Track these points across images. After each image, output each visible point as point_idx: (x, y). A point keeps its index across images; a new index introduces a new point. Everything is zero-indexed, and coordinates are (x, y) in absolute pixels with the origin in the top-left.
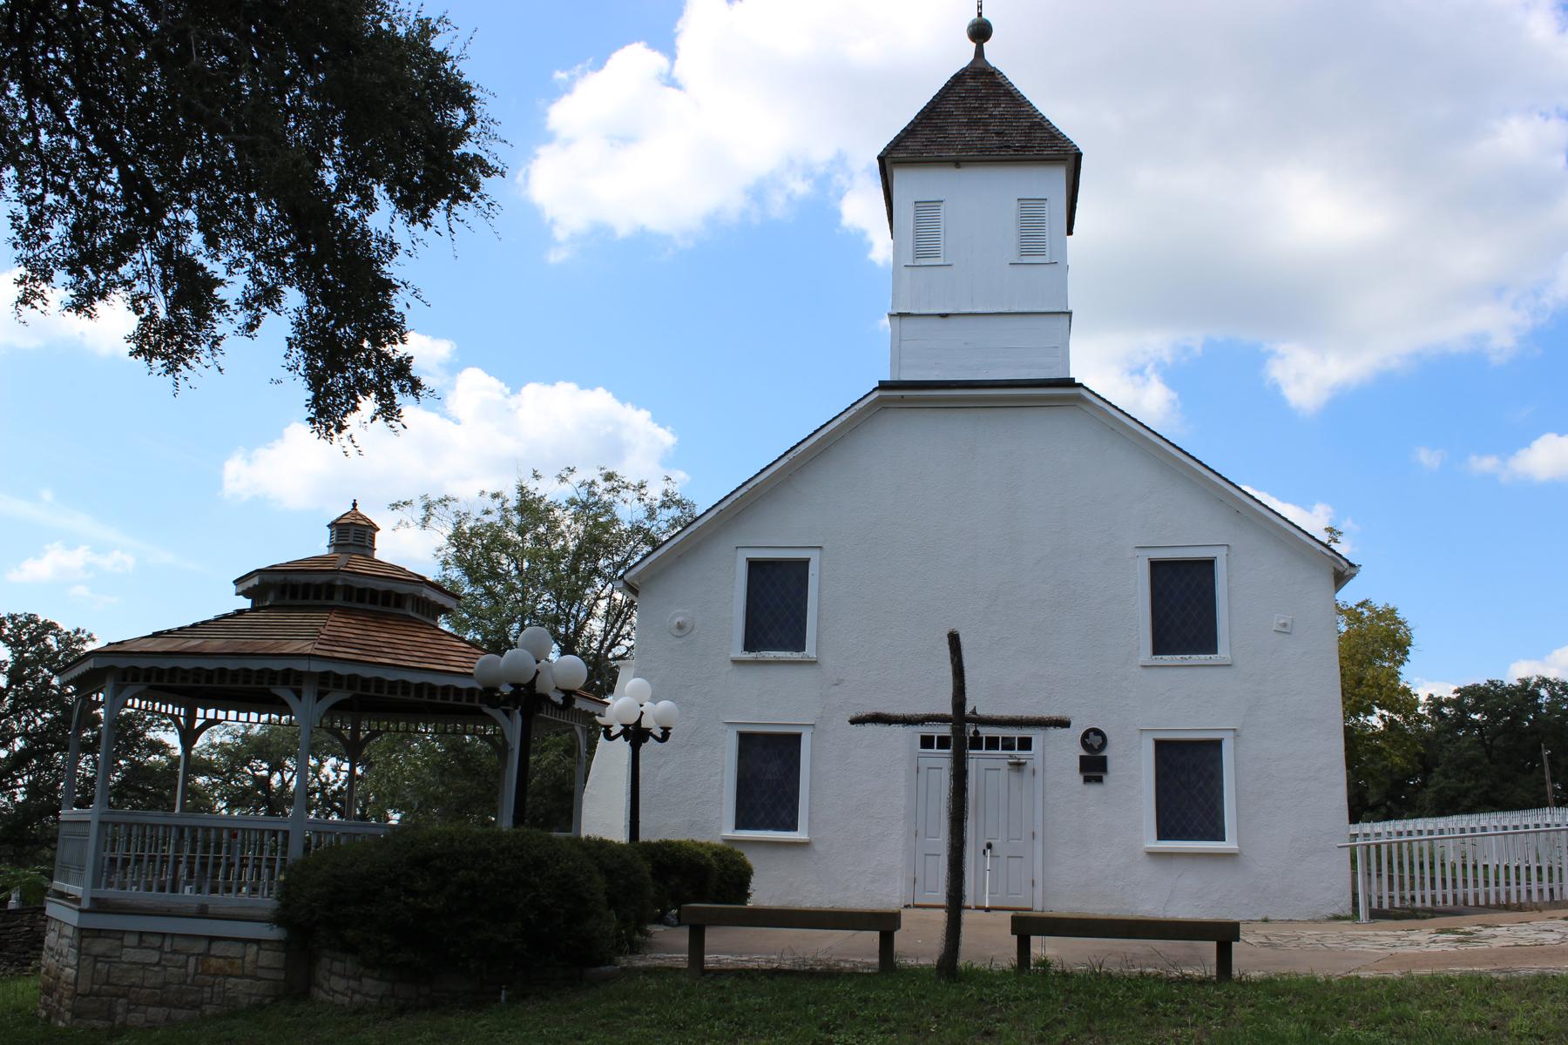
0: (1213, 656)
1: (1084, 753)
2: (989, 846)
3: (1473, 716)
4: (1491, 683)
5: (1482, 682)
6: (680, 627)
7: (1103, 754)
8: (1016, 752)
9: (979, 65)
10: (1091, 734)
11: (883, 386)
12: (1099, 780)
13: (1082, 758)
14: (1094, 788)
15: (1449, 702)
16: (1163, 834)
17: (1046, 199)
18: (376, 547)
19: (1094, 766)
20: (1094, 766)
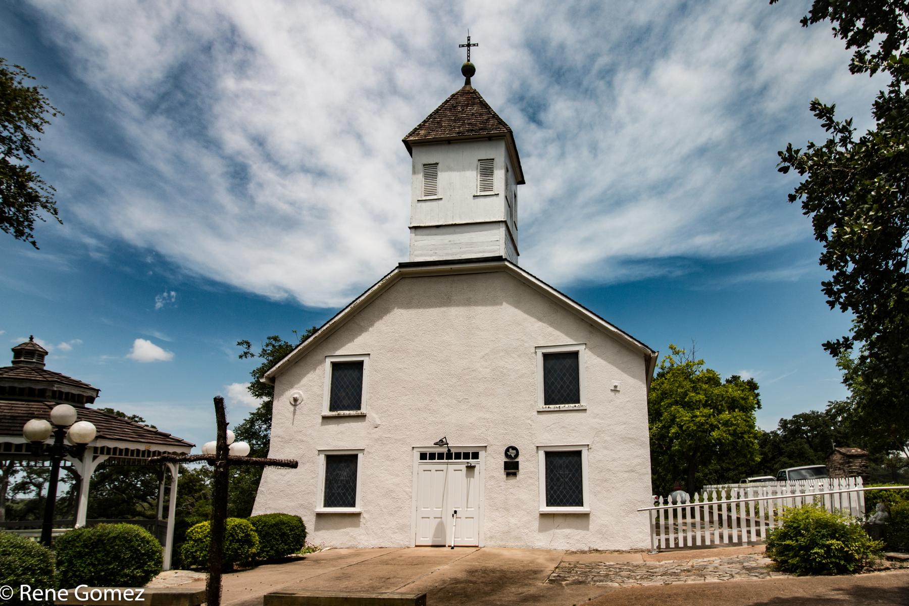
0: (577, 405)
1: (507, 460)
2: (455, 512)
3: (803, 428)
4: (813, 412)
5: (808, 412)
6: (295, 400)
7: (516, 460)
8: (470, 461)
9: (468, 88)
10: (510, 450)
11: (401, 265)
12: (515, 474)
13: (505, 462)
14: (512, 481)
15: (791, 422)
16: (550, 503)
17: (493, 159)
18: (45, 362)
19: (511, 467)
20: (511, 467)
